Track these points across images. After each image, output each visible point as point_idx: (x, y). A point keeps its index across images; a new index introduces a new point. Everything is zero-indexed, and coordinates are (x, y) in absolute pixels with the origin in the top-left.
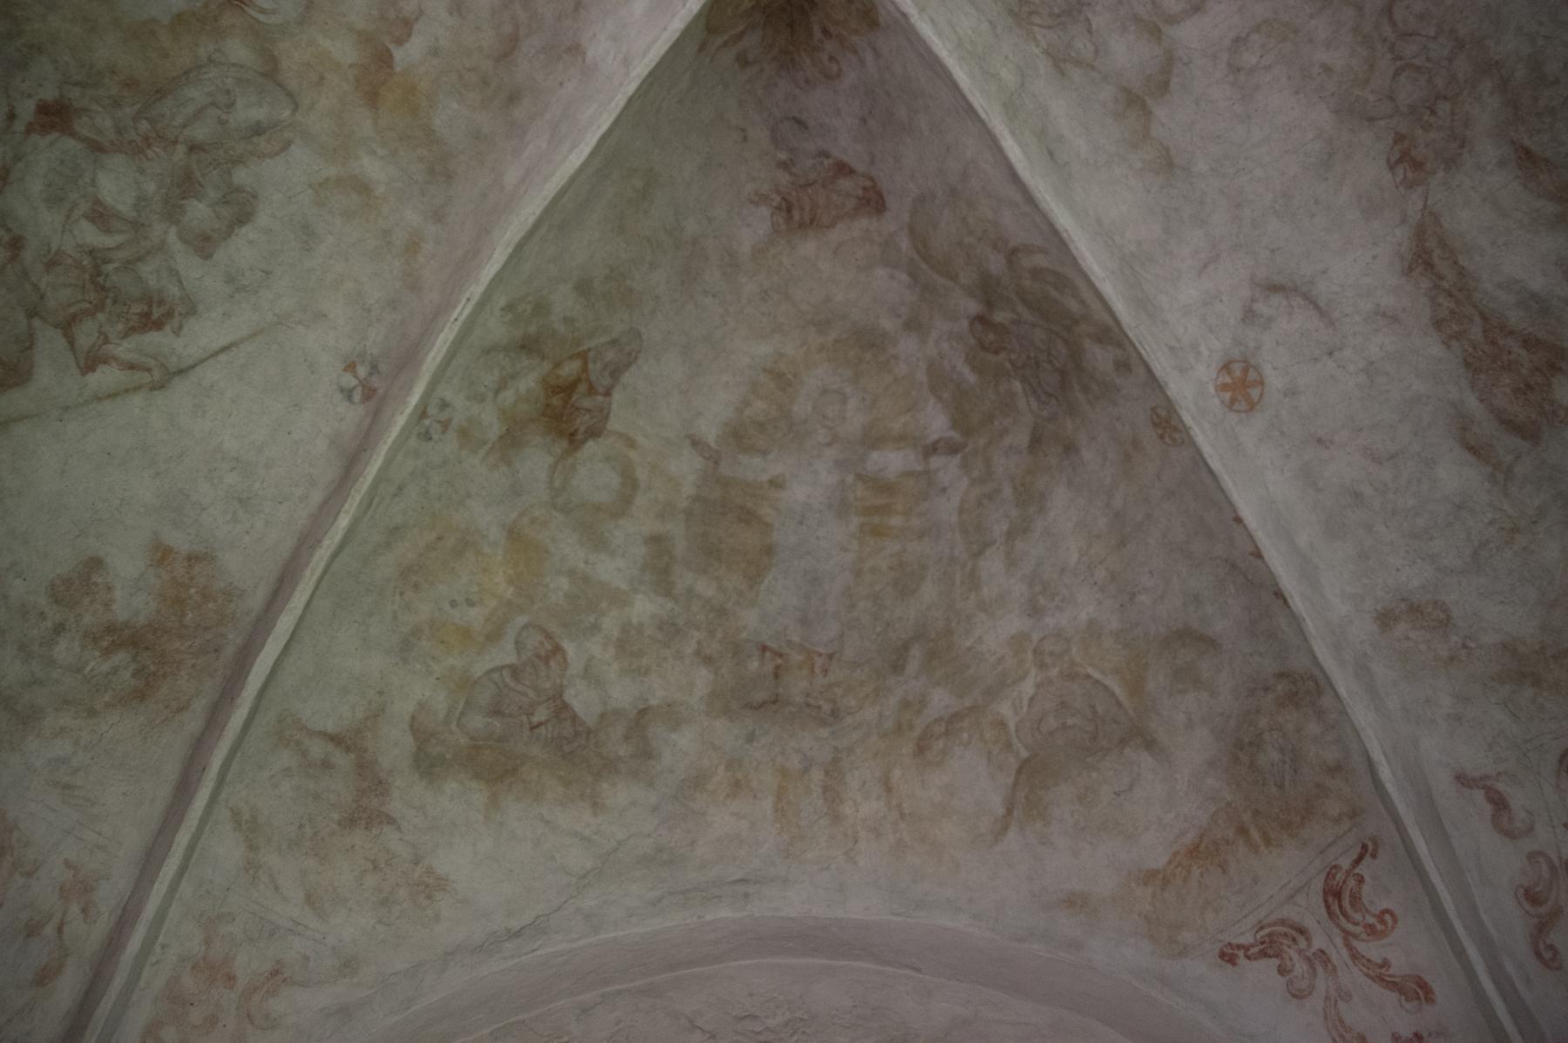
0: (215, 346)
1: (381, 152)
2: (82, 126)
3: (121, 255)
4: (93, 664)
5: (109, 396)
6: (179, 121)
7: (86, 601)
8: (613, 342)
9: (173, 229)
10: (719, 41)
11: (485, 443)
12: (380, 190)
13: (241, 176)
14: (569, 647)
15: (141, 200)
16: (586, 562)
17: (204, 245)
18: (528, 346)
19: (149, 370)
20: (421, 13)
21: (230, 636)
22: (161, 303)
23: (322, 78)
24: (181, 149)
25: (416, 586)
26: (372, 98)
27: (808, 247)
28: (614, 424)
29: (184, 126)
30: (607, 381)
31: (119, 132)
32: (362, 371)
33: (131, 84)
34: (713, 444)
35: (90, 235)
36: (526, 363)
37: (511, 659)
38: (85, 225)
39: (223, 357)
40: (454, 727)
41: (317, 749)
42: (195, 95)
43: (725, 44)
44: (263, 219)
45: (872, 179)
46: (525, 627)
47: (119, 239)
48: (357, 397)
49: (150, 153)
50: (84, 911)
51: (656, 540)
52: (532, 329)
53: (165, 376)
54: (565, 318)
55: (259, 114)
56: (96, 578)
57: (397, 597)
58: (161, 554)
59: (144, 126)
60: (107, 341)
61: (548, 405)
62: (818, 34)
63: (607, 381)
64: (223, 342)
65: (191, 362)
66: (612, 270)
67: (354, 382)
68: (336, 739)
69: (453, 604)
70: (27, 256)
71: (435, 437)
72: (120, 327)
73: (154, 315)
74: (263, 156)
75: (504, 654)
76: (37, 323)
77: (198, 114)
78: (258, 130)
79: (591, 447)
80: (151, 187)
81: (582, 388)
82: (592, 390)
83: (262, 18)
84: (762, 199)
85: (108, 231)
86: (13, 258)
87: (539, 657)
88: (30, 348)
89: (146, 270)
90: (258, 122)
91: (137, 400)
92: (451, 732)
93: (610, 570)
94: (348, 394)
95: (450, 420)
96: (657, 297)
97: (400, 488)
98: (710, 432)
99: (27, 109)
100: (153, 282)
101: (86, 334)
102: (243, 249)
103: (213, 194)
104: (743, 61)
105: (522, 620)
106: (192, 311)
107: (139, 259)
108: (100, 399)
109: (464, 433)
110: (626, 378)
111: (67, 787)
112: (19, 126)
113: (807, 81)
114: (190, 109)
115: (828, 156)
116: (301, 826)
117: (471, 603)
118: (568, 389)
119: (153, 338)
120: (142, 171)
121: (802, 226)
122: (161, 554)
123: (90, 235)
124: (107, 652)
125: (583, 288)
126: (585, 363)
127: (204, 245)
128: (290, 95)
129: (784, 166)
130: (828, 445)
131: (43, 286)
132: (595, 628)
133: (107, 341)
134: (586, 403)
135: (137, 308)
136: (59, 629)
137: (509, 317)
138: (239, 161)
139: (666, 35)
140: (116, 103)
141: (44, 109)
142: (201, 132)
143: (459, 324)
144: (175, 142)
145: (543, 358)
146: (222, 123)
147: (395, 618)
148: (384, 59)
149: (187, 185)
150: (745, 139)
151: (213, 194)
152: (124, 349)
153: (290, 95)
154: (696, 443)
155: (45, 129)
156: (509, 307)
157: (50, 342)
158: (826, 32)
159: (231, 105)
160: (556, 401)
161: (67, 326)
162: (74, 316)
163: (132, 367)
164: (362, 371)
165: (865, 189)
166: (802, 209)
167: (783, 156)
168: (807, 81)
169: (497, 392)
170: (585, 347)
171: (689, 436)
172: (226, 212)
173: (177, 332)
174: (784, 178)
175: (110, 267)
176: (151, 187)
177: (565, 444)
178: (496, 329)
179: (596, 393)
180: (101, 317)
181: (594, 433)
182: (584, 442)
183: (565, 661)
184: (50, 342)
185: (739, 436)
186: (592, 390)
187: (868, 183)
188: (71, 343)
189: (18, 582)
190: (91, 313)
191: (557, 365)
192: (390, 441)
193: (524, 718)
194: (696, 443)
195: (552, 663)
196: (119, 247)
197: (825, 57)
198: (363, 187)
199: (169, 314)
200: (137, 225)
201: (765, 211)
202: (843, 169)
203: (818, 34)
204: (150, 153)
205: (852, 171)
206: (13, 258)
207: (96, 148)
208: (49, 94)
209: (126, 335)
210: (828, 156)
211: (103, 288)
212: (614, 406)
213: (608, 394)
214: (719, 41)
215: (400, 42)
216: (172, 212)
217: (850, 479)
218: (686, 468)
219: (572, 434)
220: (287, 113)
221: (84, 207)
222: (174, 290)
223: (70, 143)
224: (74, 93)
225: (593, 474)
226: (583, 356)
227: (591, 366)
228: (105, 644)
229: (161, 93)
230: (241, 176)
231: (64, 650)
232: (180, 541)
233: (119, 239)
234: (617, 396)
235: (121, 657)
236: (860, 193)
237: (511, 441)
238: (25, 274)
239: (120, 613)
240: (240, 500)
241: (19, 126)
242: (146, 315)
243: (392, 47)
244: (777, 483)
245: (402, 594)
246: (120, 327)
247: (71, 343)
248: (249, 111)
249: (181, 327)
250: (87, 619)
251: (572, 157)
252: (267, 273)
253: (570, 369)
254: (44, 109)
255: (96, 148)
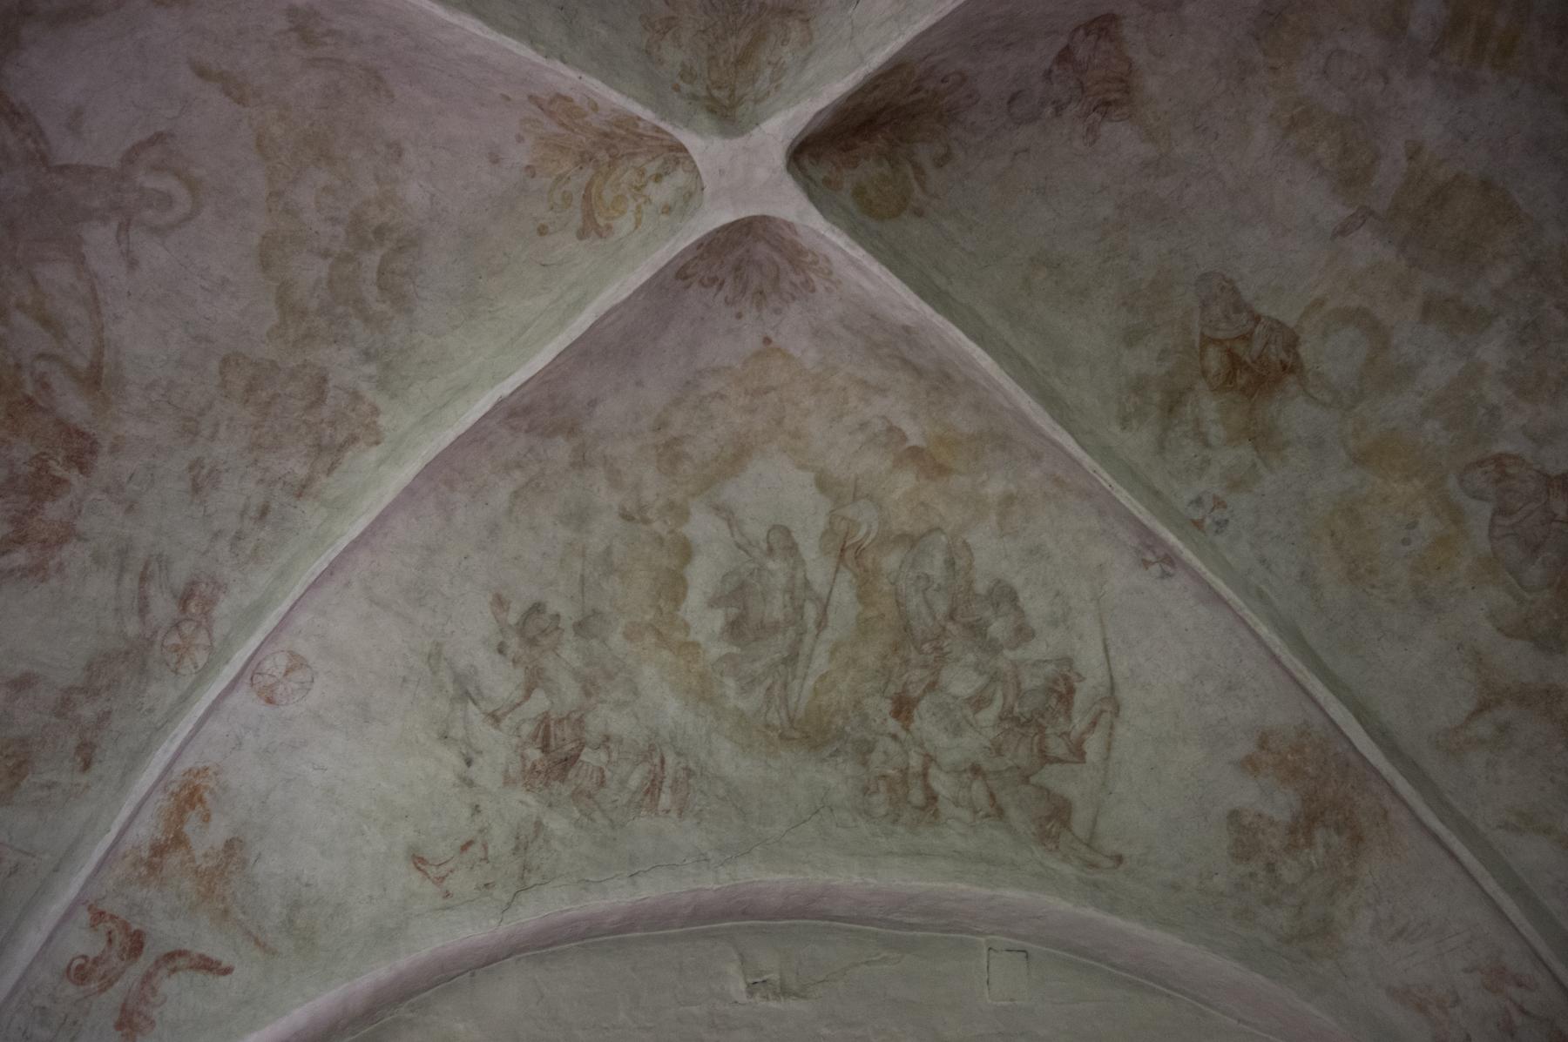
0: (1101, 654)
1: (985, 476)
2: (915, 692)
3: (1010, 699)
4: (1312, 858)
5: (1109, 749)
6: (929, 620)
7: (1260, 836)
8: (1204, 306)
9: (1006, 652)
10: (917, 192)
11: (1254, 465)
12: (1012, 488)
13: (981, 586)
14: (1502, 447)
15: (978, 668)
16: (1421, 394)
17: (1023, 633)
18: (1173, 404)
19: (1102, 712)
20: (884, 417)
21: (1339, 749)
22: (1055, 682)
23: (922, 503)
24: (950, 626)
25: (1371, 571)
26: (942, 470)
27: (1152, 85)
28: (1291, 320)
29: (934, 618)
30: (1244, 317)
31: (925, 666)
32: (1150, 557)
33: (896, 647)
34: (1351, 212)
35: (989, 715)
36: (1189, 409)
37: (1486, 510)
38: (980, 716)
39: (1112, 653)
40: (1529, 597)
41: (1483, 728)
42: (914, 602)
43: (922, 185)
44: (1017, 582)
45: (1076, 30)
46: (1461, 481)
47: (999, 695)
48: (1169, 569)
49: (947, 649)
50: (1520, 985)
51: (1429, 310)
52: (1157, 397)
53: (1111, 700)
54: (1159, 359)
55: (939, 559)
56: (1246, 821)
57: (1375, 592)
58: (1249, 765)
59: (926, 647)
60: (1067, 734)
61: (1243, 390)
62: (921, 95)
63: (1244, 317)
64: (1100, 647)
65: (1107, 678)
66: (1125, 304)
67: (1157, 566)
68: (1483, 708)
69: (1406, 542)
70: (986, 766)
71: (1226, 516)
72: (1061, 719)
73: (1062, 691)
74: (971, 566)
75: (1480, 514)
76: (1033, 780)
77: (929, 605)
78: (950, 563)
79: (1305, 351)
80: (971, 658)
81: (1240, 348)
82: (1246, 338)
83: (872, 536)
84: (1091, 129)
85: (991, 701)
86: (984, 776)
87: (1497, 481)
88: (1048, 791)
89: (1029, 683)
90: (945, 561)
91: (1120, 730)
92: (1533, 602)
93: (1439, 372)
94: (1165, 575)
95: (1215, 498)
96: (1170, 252)
97: (1263, 561)
98: (1335, 212)
99: (893, 725)
100: (1038, 682)
101: (1057, 748)
102: (1036, 606)
103: (988, 613)
104: (942, 161)
105: (1452, 483)
106: (1068, 661)
107: (1019, 684)
108: (1107, 759)
109: (1235, 486)
110: (1247, 295)
111: (1400, 933)
112: (902, 735)
113: (970, 96)
114: (924, 609)
115: (1050, 71)
116: (1552, 780)
117: (1413, 525)
118: (1235, 363)
119: (1079, 699)
120: (958, 660)
121: (1127, 91)
122: (1249, 765)
123: (989, 715)
124: (1310, 843)
125: (1131, 338)
126: (1213, 341)
127: (1023, 633)
128: (930, 531)
129: (1059, 109)
130: (1387, 80)
131: (1010, 763)
132: (1493, 411)
133: (1067, 734)
134: (1257, 346)
135: (1053, 702)
136: (1270, 867)
137: (1134, 423)
138: (970, 583)
139: (884, 278)
140: (906, 661)
141: (896, 714)
142: (942, 607)
143: (1114, 484)
144: (944, 629)
145: (1191, 389)
146: (939, 589)
147: (1393, 601)
148: (916, 453)
149: (976, 630)
150: (1026, 150)
151: (988, 613)
152: (1079, 723)
153: (930, 531)
154: (1343, 231)
155: (909, 718)
156: (1124, 422)
157: (1051, 777)
158: (917, 90)
159: (928, 577)
160: (1242, 380)
161: (1045, 758)
162: (1041, 751)
163: (1094, 724)
164: (1150, 557)
165: (1087, 34)
166: (1108, 91)
167: (1049, 111)
168: (970, 96)
169: (1207, 445)
170: (1197, 339)
171: (1334, 236)
172: (1005, 607)
173: (1081, 678)
174: (1074, 109)
175: (1017, 710)
176: (971, 658)
177: (1291, 378)
178: (1136, 442)
179: (1252, 333)
180: (1048, 731)
181: (1292, 344)
182: (1297, 356)
183: (1516, 457)
184: (1051, 777)
185: (1351, 180)
186: (1246, 338)
187: (1081, 32)
188: (1059, 761)
189: (1216, 879)
190: (1043, 737)
191: (1204, 373)
192: (1204, 569)
193: (1554, 525)
194: (1343, 231)
195: (1511, 471)
196: (1005, 697)
197: (943, 86)
198: (1009, 500)
199: (1066, 678)
200: (994, 678)
201: (1106, 128)
202: (1065, 56)
203: (921, 95)
204: (947, 649)
205: (1067, 47)
206: (984, 776)
207: (932, 686)
208: (887, 706)
209: (1069, 718)
210: (1050, 71)
211: (1029, 721)
212: (1273, 314)
213: (1257, 319)
214: (917, 192)
215: (904, 438)
216: (993, 648)
217: (1433, 65)
218: (1366, 249)
219: (1284, 368)
220: (943, 538)
221: (969, 712)
222: (1050, 668)
223: (924, 704)
224: (892, 689)
225: (1333, 355)
226: (1207, 341)
227: (1220, 335)
228: (1302, 841)
229: (907, 628)
230: (981, 586)
231: (1289, 872)
232: (1244, 747)
233: (999, 695)
234: (1263, 309)
235: (1319, 835)
236: (1092, 38)
237: (1263, 439)
238: (998, 773)
239: (1284, 817)
240: (1230, 688)
241: (902, 735)
242: (1061, 697)
243: (907, 445)
244: (1414, 153)
245: (1373, 586)
246: (1061, 719)
247: (1059, 761)
248: (935, 567)
249: (1079, 675)
250: (1275, 843)
251: (983, 364)
252: (1058, 594)
253: (1214, 359)
254: (896, 714)
255: (932, 686)
